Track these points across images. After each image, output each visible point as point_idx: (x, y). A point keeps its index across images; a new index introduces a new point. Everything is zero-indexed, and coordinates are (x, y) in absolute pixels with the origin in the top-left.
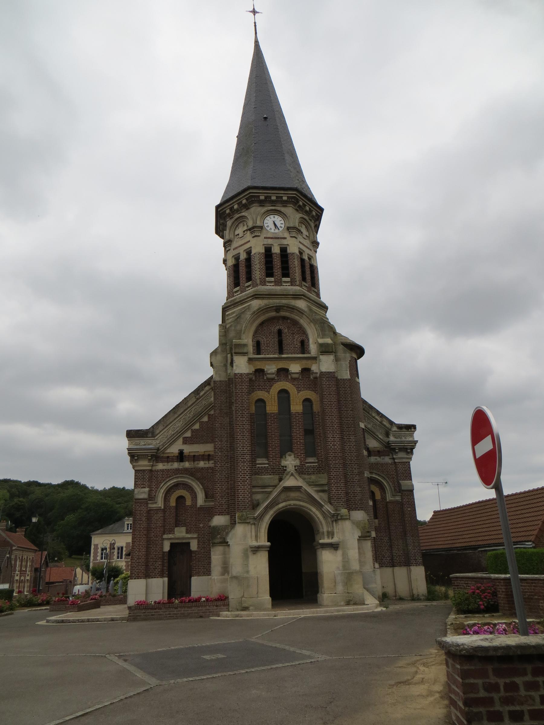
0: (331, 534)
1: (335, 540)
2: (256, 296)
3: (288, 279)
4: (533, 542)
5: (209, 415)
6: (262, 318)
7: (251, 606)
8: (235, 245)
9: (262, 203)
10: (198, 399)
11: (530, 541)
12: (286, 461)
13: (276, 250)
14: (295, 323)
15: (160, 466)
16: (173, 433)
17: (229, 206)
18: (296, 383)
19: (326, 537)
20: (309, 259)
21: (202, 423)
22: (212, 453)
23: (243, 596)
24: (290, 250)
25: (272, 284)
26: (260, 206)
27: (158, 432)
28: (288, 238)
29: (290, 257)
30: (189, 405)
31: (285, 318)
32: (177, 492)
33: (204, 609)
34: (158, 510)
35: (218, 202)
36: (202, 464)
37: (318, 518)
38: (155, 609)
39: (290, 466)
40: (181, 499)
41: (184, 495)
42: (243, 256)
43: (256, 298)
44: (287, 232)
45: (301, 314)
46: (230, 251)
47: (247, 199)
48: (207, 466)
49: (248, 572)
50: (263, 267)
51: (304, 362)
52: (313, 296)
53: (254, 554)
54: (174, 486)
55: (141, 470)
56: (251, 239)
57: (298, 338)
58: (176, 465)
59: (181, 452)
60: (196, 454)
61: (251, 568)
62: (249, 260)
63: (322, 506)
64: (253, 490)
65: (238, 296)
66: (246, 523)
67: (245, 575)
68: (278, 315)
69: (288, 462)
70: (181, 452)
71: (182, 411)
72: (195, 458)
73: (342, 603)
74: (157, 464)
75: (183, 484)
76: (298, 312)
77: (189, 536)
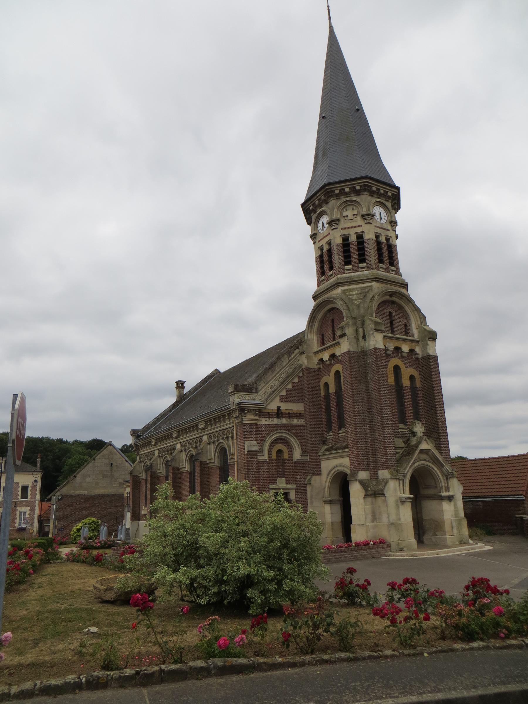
0: (447, 489)
1: (451, 493)
2: (377, 279)
3: (364, 265)
4: (524, 496)
5: (299, 376)
6: (320, 316)
7: (405, 547)
8: (319, 237)
9: (372, 193)
10: (290, 360)
11: (521, 495)
12: (416, 427)
13: (353, 239)
14: (401, 308)
15: (264, 421)
16: (271, 390)
17: (339, 187)
18: (404, 360)
19: (444, 491)
20: (388, 240)
21: (293, 383)
22: (303, 412)
23: (399, 540)
24: (366, 237)
25: (383, 270)
26: (370, 195)
27: (260, 388)
28: (363, 225)
29: (366, 243)
30: (284, 365)
31: (393, 302)
32: (277, 446)
33: (374, 550)
34: (265, 462)
35: (302, 200)
36: (295, 422)
37: (438, 476)
38: (342, 552)
39: (419, 432)
40: (280, 452)
41: (282, 449)
42: (326, 248)
43: (376, 281)
44: (389, 224)
45: (408, 302)
46: (338, 229)
47: (361, 186)
48: (299, 423)
49: (399, 519)
50: (341, 256)
51: (411, 343)
52: (391, 275)
53: (402, 504)
54: (275, 440)
55: (249, 424)
56: (363, 224)
57: (403, 322)
58: (276, 421)
59: (279, 408)
60: (291, 412)
61: (402, 515)
62: (330, 251)
63: (443, 466)
64: (397, 451)
65: (324, 286)
66: (396, 478)
67: (399, 522)
68: (390, 299)
69: (417, 429)
70: (279, 408)
71: (278, 370)
72: (290, 415)
73: (457, 543)
74: (261, 419)
75: (281, 439)
76: (406, 300)
77: (289, 486)
